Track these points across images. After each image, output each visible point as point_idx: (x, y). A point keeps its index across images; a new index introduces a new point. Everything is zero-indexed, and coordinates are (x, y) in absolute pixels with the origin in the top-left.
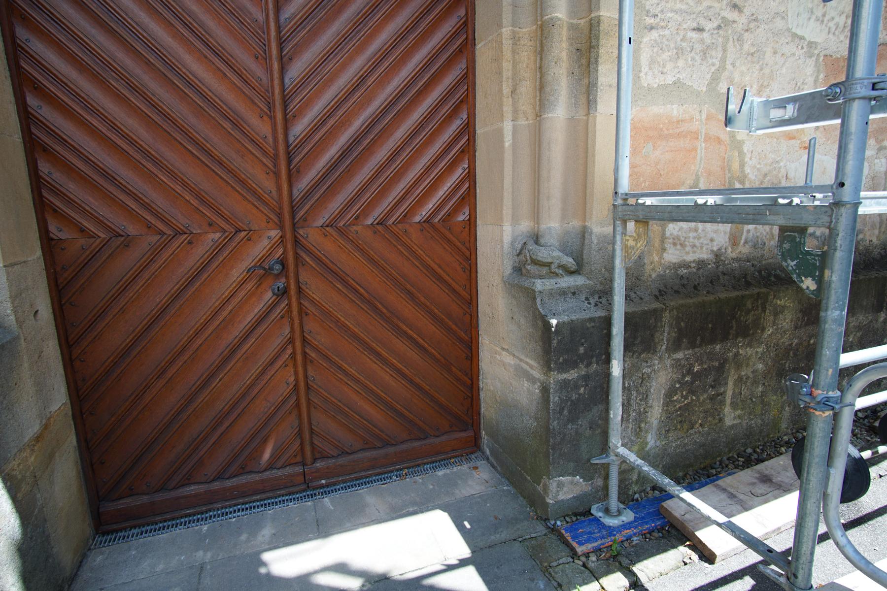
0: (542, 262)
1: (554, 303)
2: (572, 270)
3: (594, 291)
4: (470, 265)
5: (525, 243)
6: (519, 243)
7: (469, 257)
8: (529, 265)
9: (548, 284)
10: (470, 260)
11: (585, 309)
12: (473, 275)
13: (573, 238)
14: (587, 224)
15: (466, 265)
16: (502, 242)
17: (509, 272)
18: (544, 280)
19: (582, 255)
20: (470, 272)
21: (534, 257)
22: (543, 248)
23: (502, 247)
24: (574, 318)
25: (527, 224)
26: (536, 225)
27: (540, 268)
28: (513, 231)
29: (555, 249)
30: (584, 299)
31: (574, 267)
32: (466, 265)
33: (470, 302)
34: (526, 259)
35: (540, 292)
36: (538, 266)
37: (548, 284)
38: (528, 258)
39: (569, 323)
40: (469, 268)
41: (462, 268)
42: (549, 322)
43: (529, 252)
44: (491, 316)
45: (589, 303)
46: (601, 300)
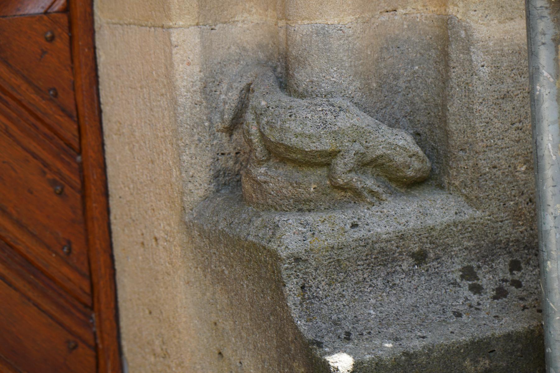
0: (302, 151)
1: (348, 294)
2: (410, 173)
3: (494, 243)
4: (81, 170)
5: (248, 89)
6: (230, 88)
7: (76, 146)
8: (260, 163)
9: (325, 228)
10: (80, 153)
11: (461, 308)
12: (94, 207)
13: (412, 62)
14: (451, 10)
15: (65, 171)
16: (171, 85)
17: (201, 192)
18: (310, 218)
19: (444, 120)
20: (84, 197)
21: (274, 136)
22: (304, 102)
23: (174, 102)
24: (416, 345)
25: (255, 18)
26: (282, 23)
27: (298, 175)
28: (206, 46)
29: (346, 103)
30: (457, 276)
31: (417, 165)
32: (65, 171)
33: (87, 299)
34: (250, 142)
35: (297, 260)
36: (289, 167)
37: (325, 228)
38: (256, 140)
39: (397, 364)
40: (76, 180)
41: (54, 183)
42: (326, 365)
43: (258, 116)
44: (158, 350)
45: (476, 289)
46: (517, 275)
